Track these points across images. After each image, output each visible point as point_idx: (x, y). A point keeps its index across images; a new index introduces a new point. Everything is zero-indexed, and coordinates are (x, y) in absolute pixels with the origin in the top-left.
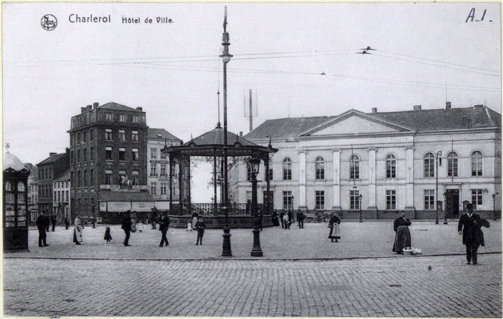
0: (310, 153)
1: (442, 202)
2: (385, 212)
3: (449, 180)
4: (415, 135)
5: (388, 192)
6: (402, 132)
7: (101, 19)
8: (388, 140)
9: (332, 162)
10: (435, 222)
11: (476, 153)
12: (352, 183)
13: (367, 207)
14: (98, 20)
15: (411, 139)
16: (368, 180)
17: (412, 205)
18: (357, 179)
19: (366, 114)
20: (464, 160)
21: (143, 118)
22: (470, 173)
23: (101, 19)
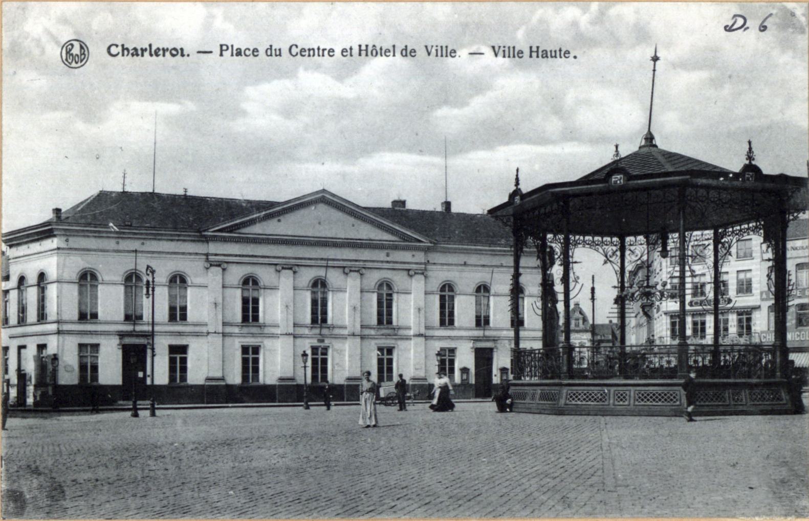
0: (368, 273)
1: (507, 369)
2: (240, 388)
3: (479, 333)
4: (427, 250)
5: (245, 350)
6: (406, 243)
7: (326, 52)
8: (381, 255)
9: (426, 293)
10: (397, 407)
11: (483, 289)
12: (317, 331)
13: (204, 377)
14: (307, 53)
15: (420, 257)
16: (277, 326)
17: (219, 374)
18: (324, 325)
19: (365, 208)
20: (112, 288)
21: (113, 195)
22: (76, 317)
23: (326, 52)
